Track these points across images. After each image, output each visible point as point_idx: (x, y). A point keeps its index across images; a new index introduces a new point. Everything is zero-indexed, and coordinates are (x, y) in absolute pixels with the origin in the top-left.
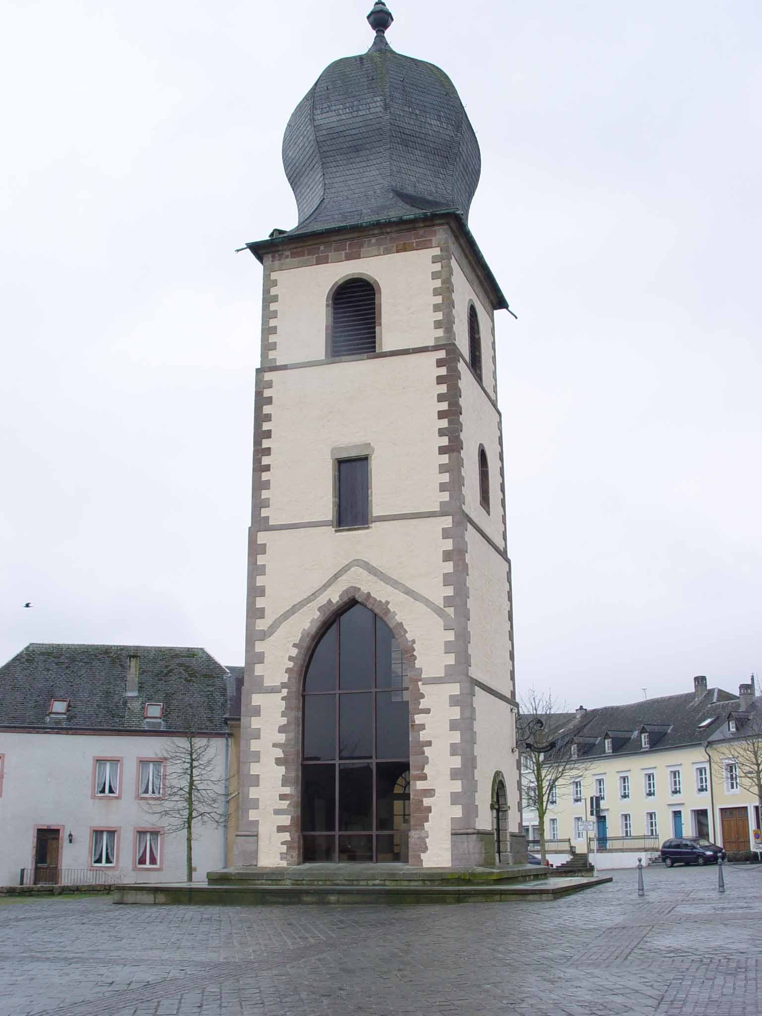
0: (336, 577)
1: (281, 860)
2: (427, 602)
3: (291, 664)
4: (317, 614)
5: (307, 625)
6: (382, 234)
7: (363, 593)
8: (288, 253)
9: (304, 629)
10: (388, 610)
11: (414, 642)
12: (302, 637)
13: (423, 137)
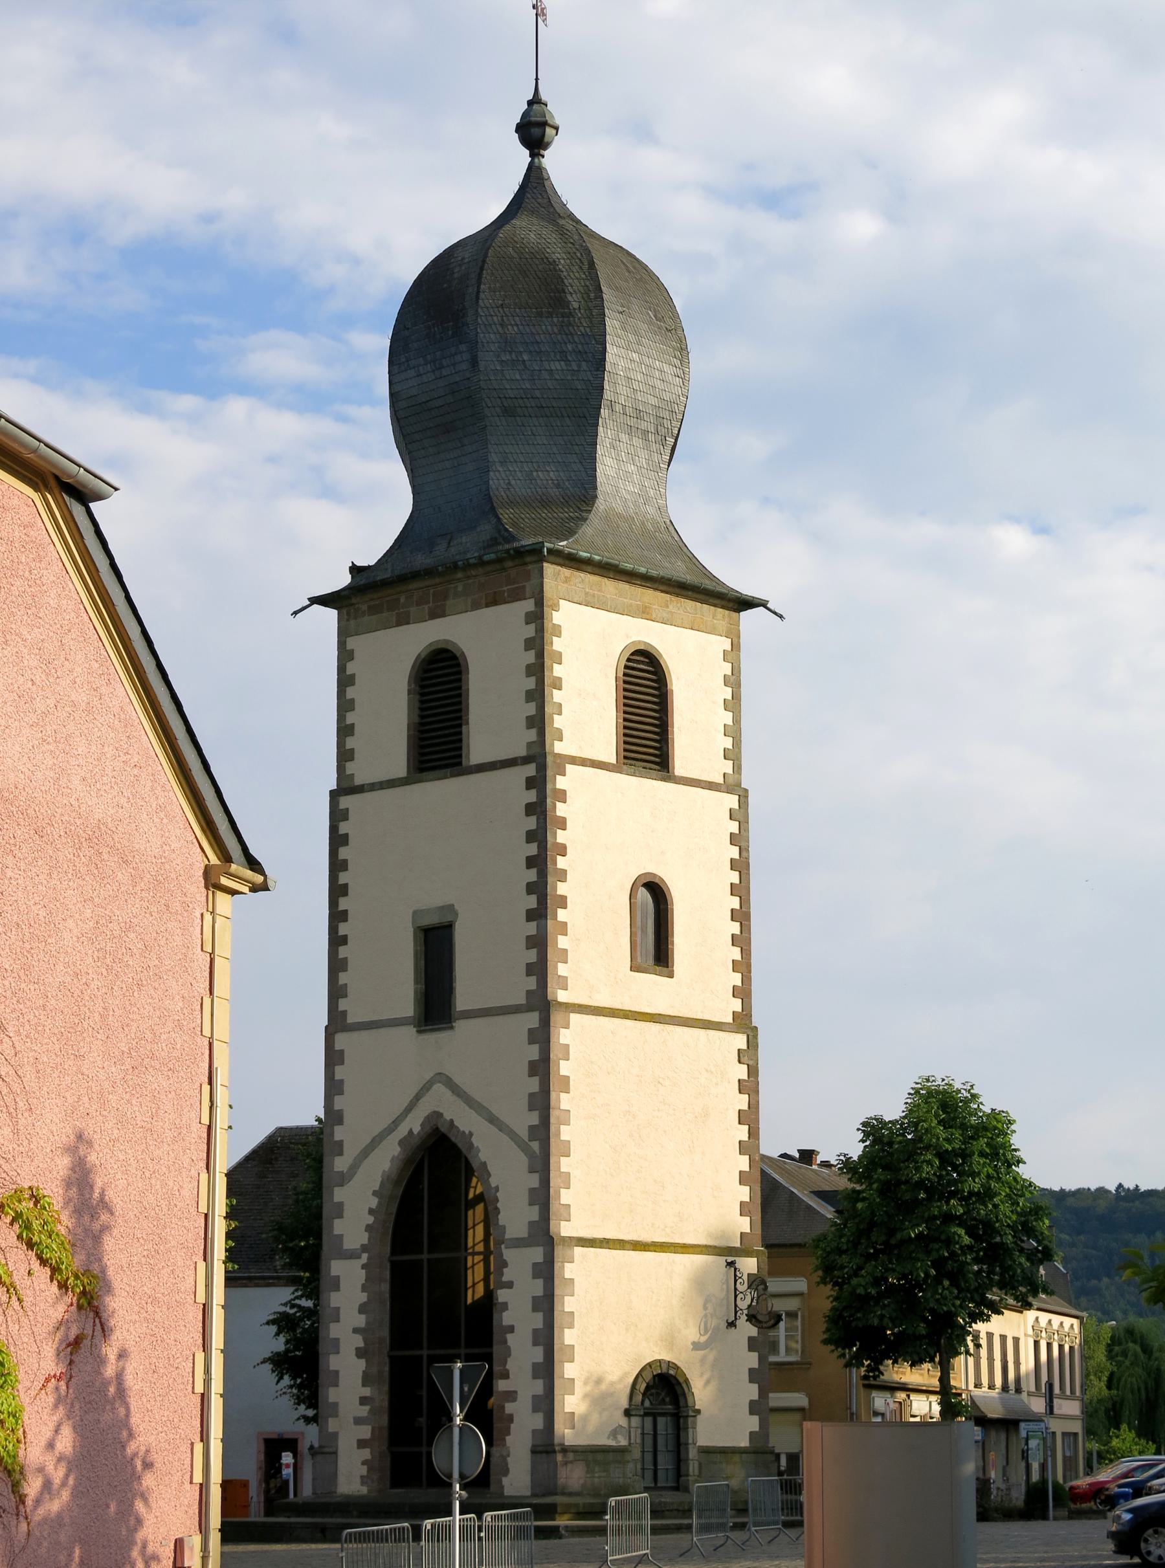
0: (417, 1098)
1: (362, 1485)
2: (512, 1135)
3: (370, 1220)
4: (396, 1150)
5: (386, 1165)
6: (468, 577)
7: (446, 1120)
8: (364, 607)
9: (384, 1171)
10: (472, 1144)
11: (497, 1189)
12: (382, 1182)
13: (539, 396)
